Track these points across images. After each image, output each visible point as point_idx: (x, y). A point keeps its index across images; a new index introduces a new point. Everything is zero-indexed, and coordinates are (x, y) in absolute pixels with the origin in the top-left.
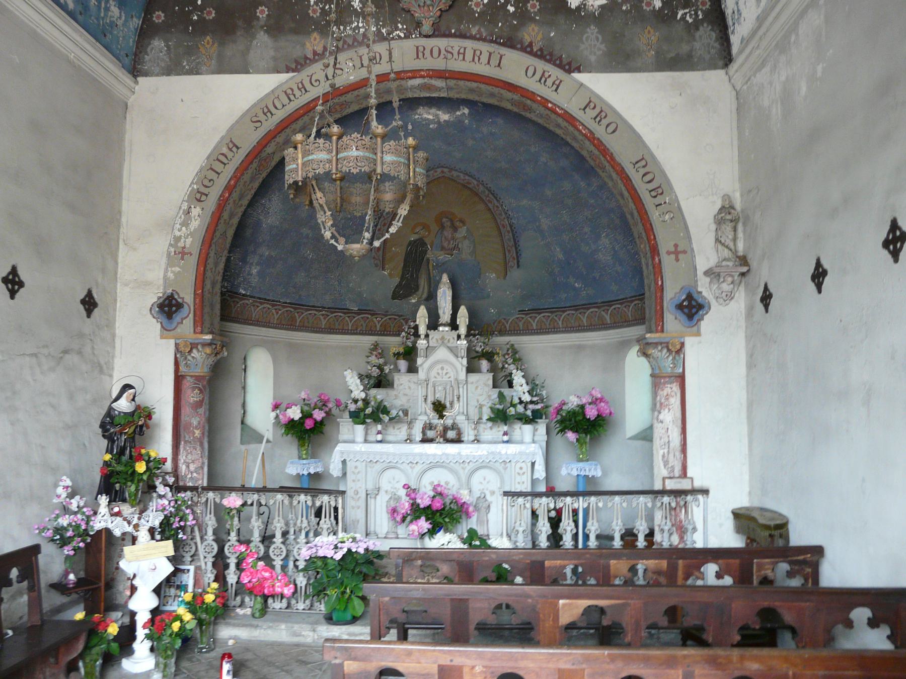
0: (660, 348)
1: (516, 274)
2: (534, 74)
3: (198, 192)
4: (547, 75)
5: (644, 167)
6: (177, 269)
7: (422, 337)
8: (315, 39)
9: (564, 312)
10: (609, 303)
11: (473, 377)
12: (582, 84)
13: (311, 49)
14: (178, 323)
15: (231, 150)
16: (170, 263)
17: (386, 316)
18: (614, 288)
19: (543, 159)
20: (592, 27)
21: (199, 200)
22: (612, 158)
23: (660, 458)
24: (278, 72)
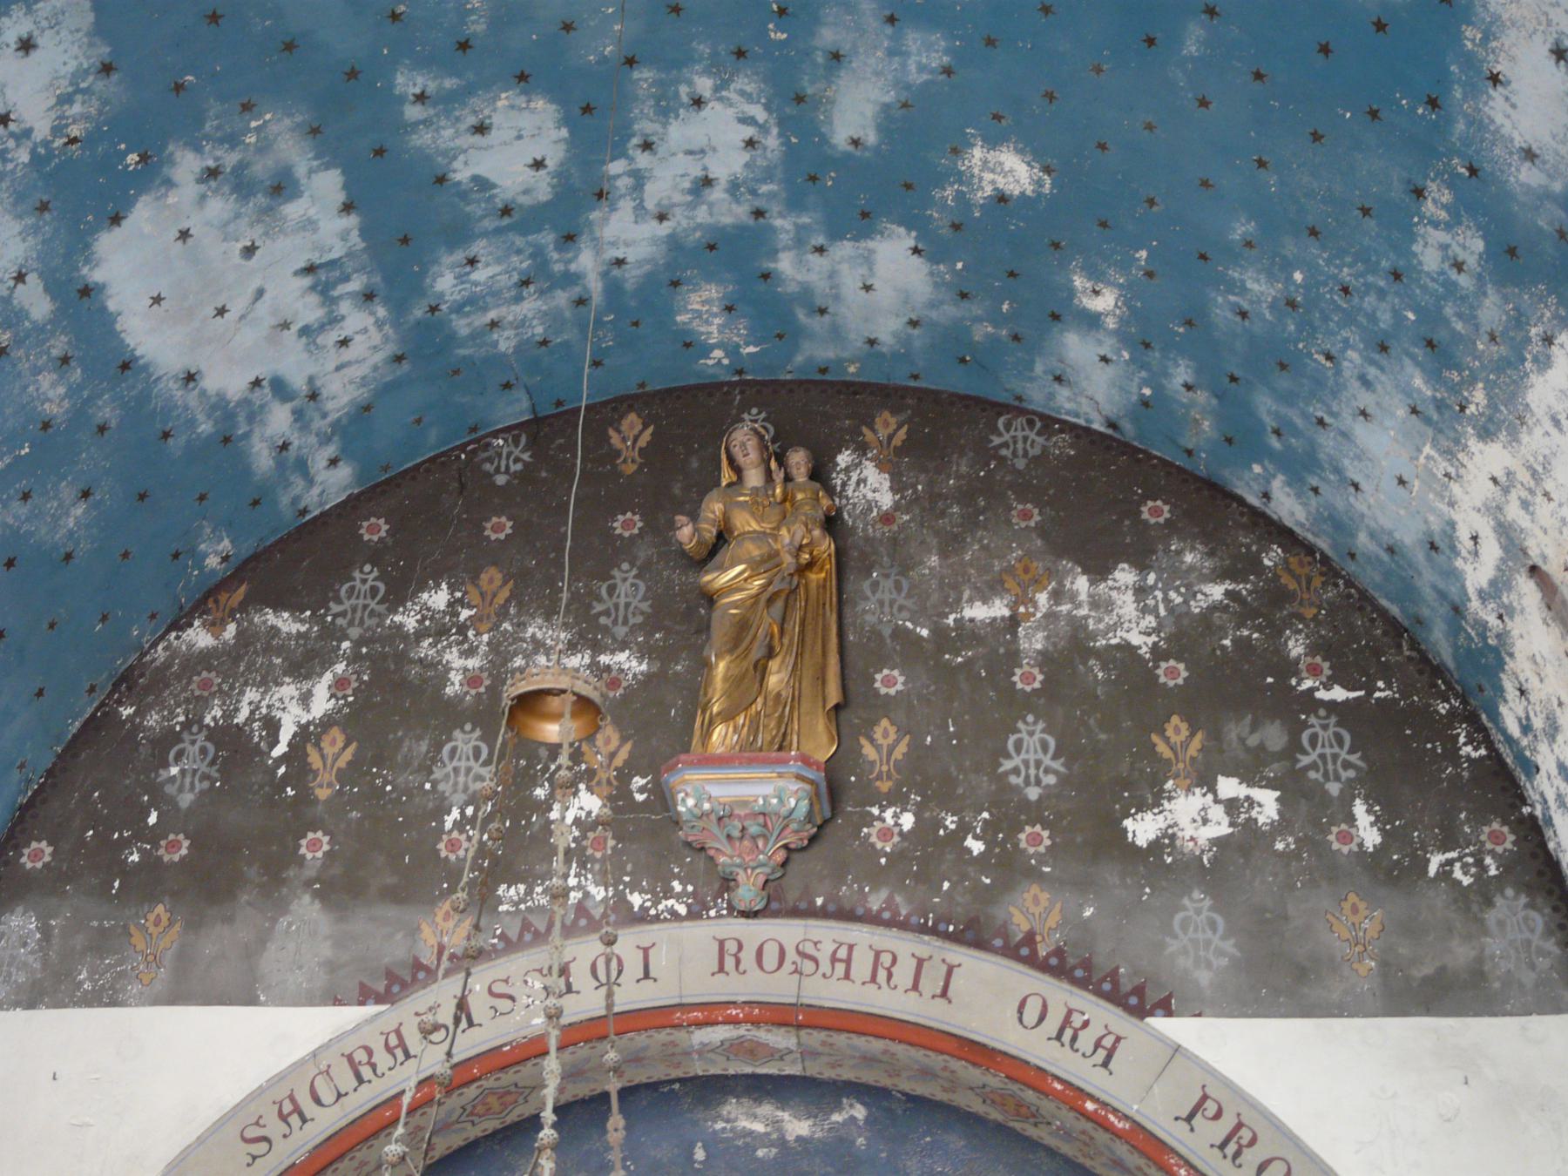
2: (1042, 1019)
4: (1077, 1021)
13: (433, 941)
24: (337, 1002)
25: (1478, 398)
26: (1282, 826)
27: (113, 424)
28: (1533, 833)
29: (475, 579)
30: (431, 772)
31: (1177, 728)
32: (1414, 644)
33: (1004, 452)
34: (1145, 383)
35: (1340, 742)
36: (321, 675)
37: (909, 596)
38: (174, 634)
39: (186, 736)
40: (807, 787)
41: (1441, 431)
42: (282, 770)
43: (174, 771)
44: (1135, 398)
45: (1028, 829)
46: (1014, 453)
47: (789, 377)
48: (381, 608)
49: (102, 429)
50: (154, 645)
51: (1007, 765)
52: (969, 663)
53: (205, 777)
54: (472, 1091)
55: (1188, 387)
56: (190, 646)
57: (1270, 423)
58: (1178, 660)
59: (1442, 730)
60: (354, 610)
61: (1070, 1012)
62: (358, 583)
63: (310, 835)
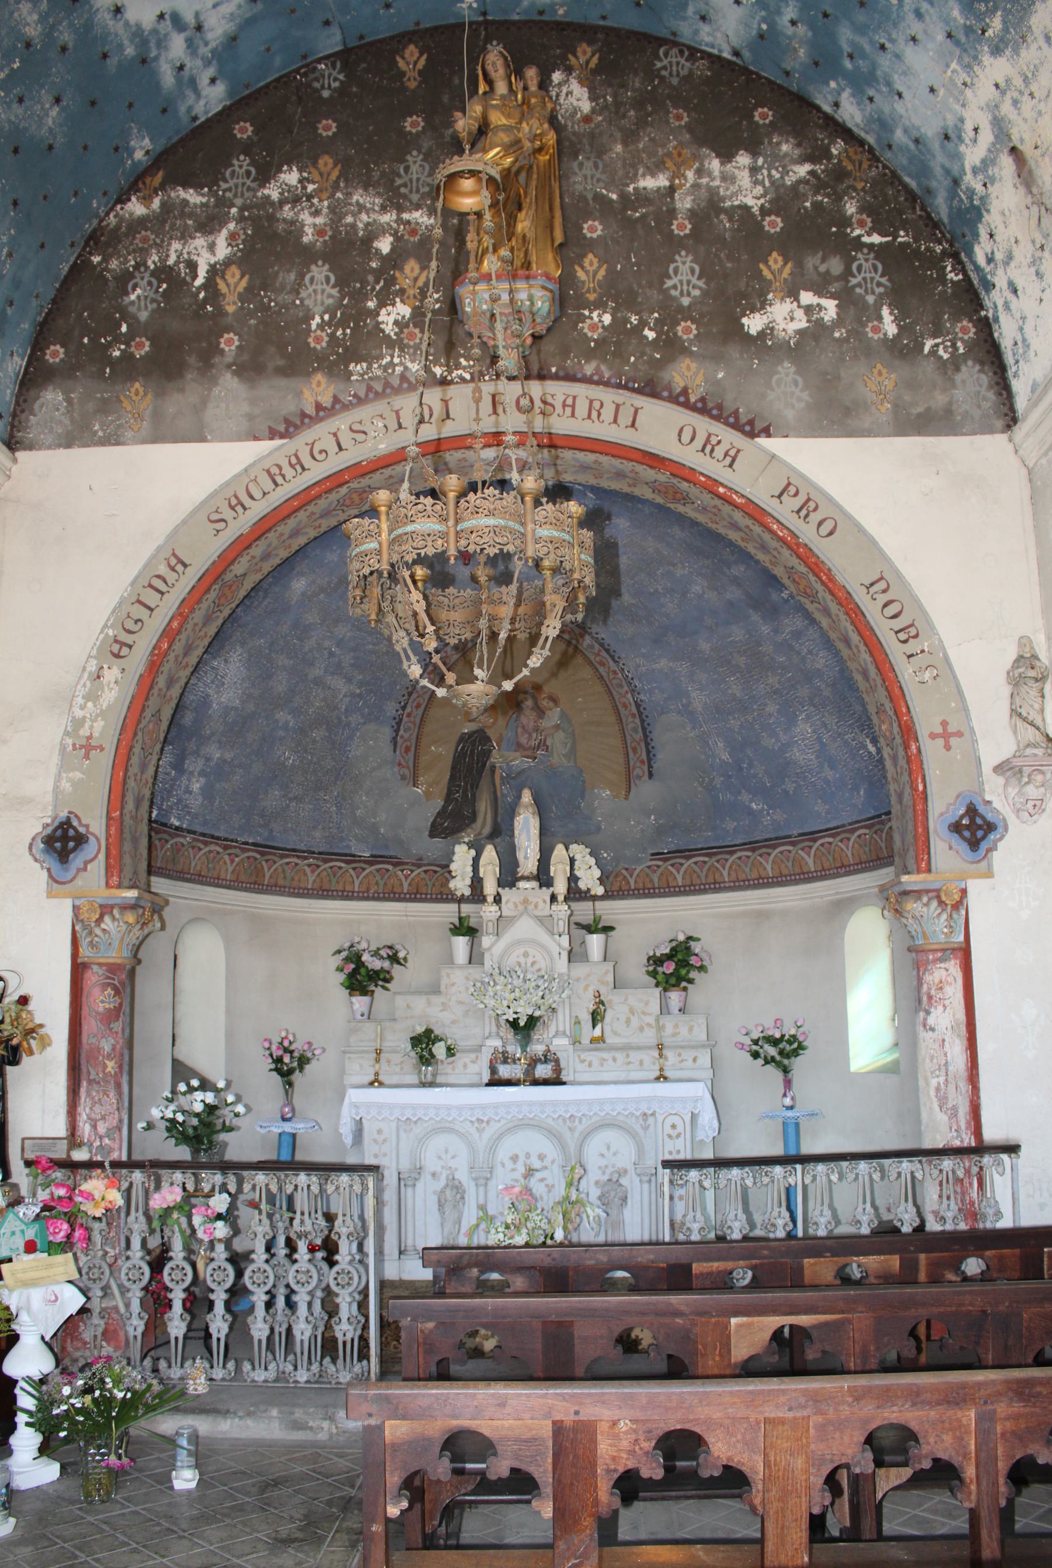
0: (925, 899)
1: (646, 791)
2: (692, 439)
3: (116, 641)
4: (714, 440)
5: (884, 591)
6: (78, 775)
7: (490, 899)
8: (319, 384)
9: (732, 853)
10: (812, 836)
11: (580, 970)
12: (774, 456)
13: (311, 400)
14: (79, 870)
15: (173, 569)
16: (65, 764)
17: (419, 866)
18: (820, 807)
19: (697, 589)
20: (787, 364)
21: (117, 656)
22: (831, 579)
23: (932, 1093)
24: (256, 438)
25: (996, 24)
26: (838, 323)
27: (71, 45)
28: (986, 327)
29: (315, 164)
30: (298, 293)
31: (775, 260)
32: (923, 208)
33: (663, 73)
34: (764, 20)
35: (876, 270)
36: (219, 231)
37: (603, 172)
38: (119, 207)
39: (137, 274)
40: (548, 294)
41: (965, 50)
42: (202, 295)
43: (133, 297)
44: (754, 32)
45: (683, 324)
46: (671, 74)
47: (516, 17)
48: (254, 185)
49: (64, 49)
50: (107, 214)
51: (669, 283)
52: (644, 216)
53: (153, 301)
54: (344, 490)
55: (793, 23)
56: (131, 214)
57: (847, 48)
58: (777, 215)
59: (935, 262)
60: (236, 186)
61: (709, 435)
62: (237, 168)
63: (226, 336)
